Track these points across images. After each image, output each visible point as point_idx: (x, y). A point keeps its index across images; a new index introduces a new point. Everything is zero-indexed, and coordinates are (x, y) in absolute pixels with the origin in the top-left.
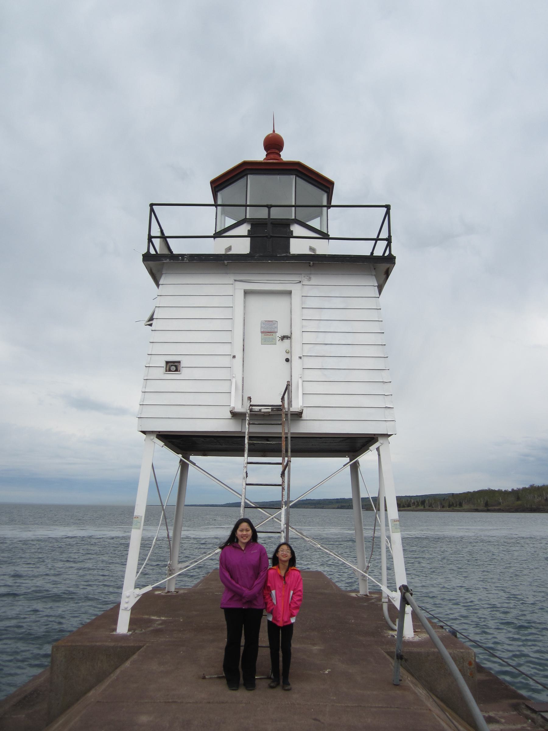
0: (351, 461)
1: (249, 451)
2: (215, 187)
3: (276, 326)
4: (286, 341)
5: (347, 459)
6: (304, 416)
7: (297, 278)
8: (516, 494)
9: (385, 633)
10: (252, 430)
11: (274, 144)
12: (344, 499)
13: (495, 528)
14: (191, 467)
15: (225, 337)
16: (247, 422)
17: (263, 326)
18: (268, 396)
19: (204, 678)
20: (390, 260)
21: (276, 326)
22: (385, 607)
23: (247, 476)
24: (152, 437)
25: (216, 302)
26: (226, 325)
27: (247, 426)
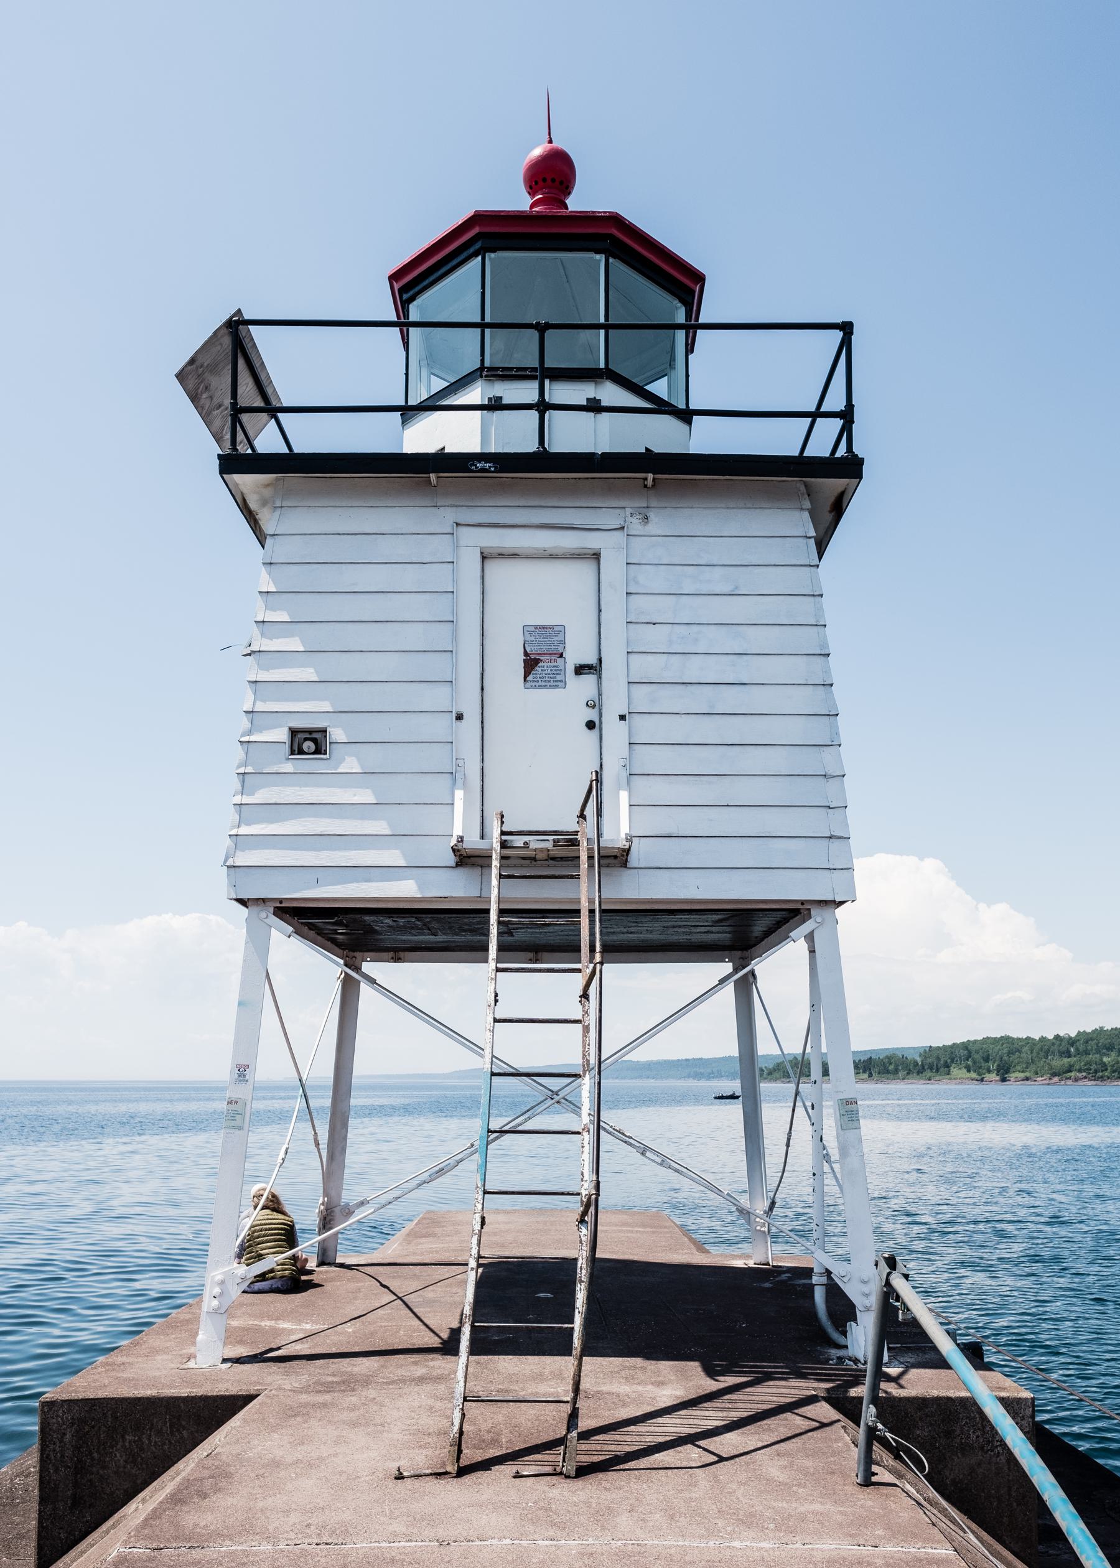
0: (736, 970)
1: (501, 948)
2: (402, 290)
3: (560, 637)
4: (589, 679)
5: (727, 967)
6: (633, 860)
7: (611, 519)
8: (1063, 1046)
9: (821, 1353)
10: (506, 894)
11: (552, 173)
12: (701, 1059)
13: (72, 1108)
14: (365, 988)
15: (438, 667)
16: (495, 872)
17: (529, 638)
18: (543, 804)
19: (400, 1477)
20: (850, 467)
21: (560, 637)
22: (819, 1295)
23: (496, 1001)
24: (263, 915)
25: (409, 578)
26: (440, 637)
27: (495, 882)
